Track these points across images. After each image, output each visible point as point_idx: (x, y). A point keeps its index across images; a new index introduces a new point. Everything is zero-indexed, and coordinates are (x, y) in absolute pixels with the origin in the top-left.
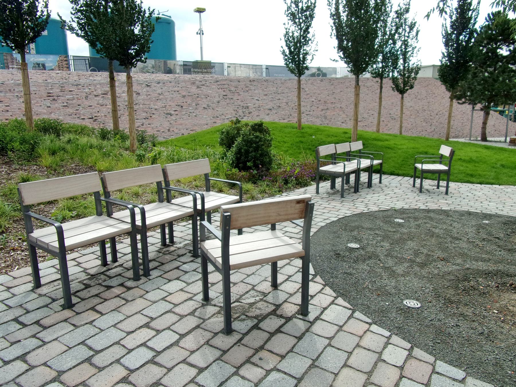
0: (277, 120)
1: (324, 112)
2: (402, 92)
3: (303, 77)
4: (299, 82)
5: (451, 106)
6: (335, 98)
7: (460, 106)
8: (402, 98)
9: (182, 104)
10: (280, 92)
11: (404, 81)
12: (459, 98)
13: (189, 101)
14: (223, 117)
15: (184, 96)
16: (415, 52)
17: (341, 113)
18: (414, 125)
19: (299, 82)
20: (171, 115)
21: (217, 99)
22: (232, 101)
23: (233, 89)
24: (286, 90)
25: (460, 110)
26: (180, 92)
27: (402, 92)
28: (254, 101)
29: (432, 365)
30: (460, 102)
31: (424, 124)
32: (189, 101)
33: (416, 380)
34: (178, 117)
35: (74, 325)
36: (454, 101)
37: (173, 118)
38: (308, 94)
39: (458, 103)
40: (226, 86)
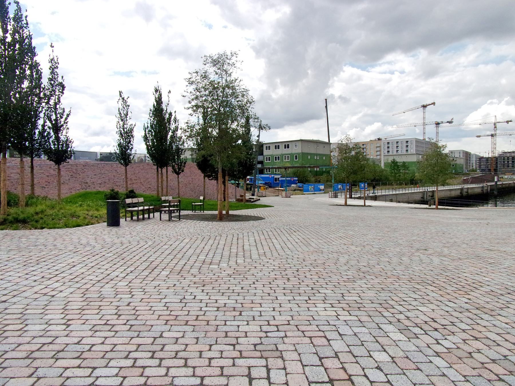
0: (106, 191)
1: (131, 185)
2: (178, 174)
3: (128, 167)
4: (126, 169)
5: (204, 181)
6: (136, 177)
7: (211, 181)
8: (178, 177)
9: (49, 181)
10: (103, 172)
11: (178, 167)
12: (209, 177)
13: (52, 179)
14: (75, 189)
15: (48, 176)
16: (183, 152)
17: (142, 186)
18: (185, 193)
19: (126, 169)
20: (45, 188)
21: (67, 178)
22: (77, 179)
23: (74, 171)
24: (106, 172)
25: (211, 183)
26: (45, 173)
27: (178, 174)
28: (90, 179)
29: (280, 357)
30: (210, 179)
31: (191, 192)
32: (52, 179)
33: (314, 364)
34: (49, 189)
35: (298, 329)
36: (206, 178)
37: (46, 189)
38: (119, 174)
39: (209, 179)
40: (70, 169)
